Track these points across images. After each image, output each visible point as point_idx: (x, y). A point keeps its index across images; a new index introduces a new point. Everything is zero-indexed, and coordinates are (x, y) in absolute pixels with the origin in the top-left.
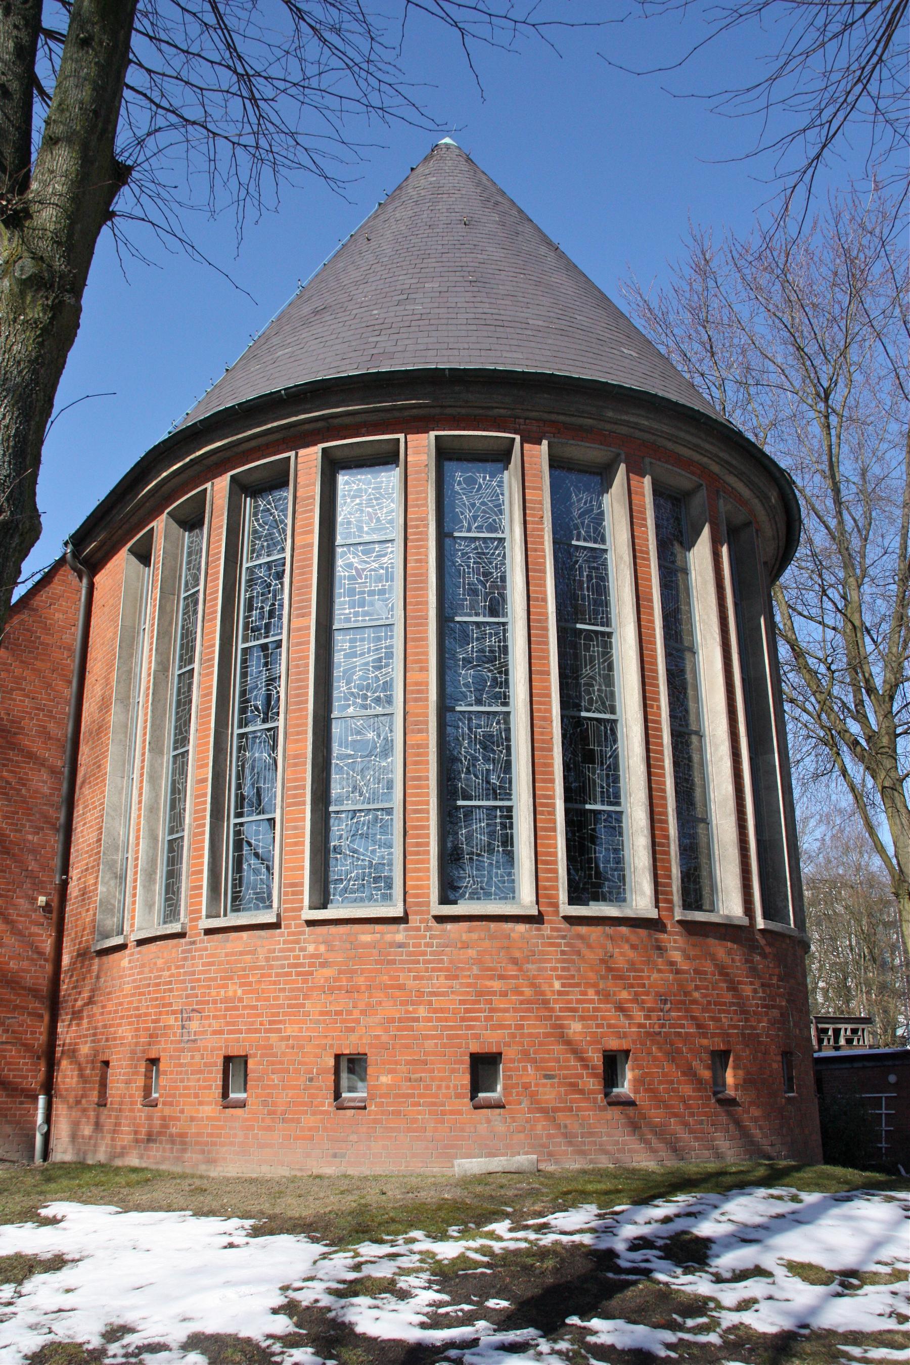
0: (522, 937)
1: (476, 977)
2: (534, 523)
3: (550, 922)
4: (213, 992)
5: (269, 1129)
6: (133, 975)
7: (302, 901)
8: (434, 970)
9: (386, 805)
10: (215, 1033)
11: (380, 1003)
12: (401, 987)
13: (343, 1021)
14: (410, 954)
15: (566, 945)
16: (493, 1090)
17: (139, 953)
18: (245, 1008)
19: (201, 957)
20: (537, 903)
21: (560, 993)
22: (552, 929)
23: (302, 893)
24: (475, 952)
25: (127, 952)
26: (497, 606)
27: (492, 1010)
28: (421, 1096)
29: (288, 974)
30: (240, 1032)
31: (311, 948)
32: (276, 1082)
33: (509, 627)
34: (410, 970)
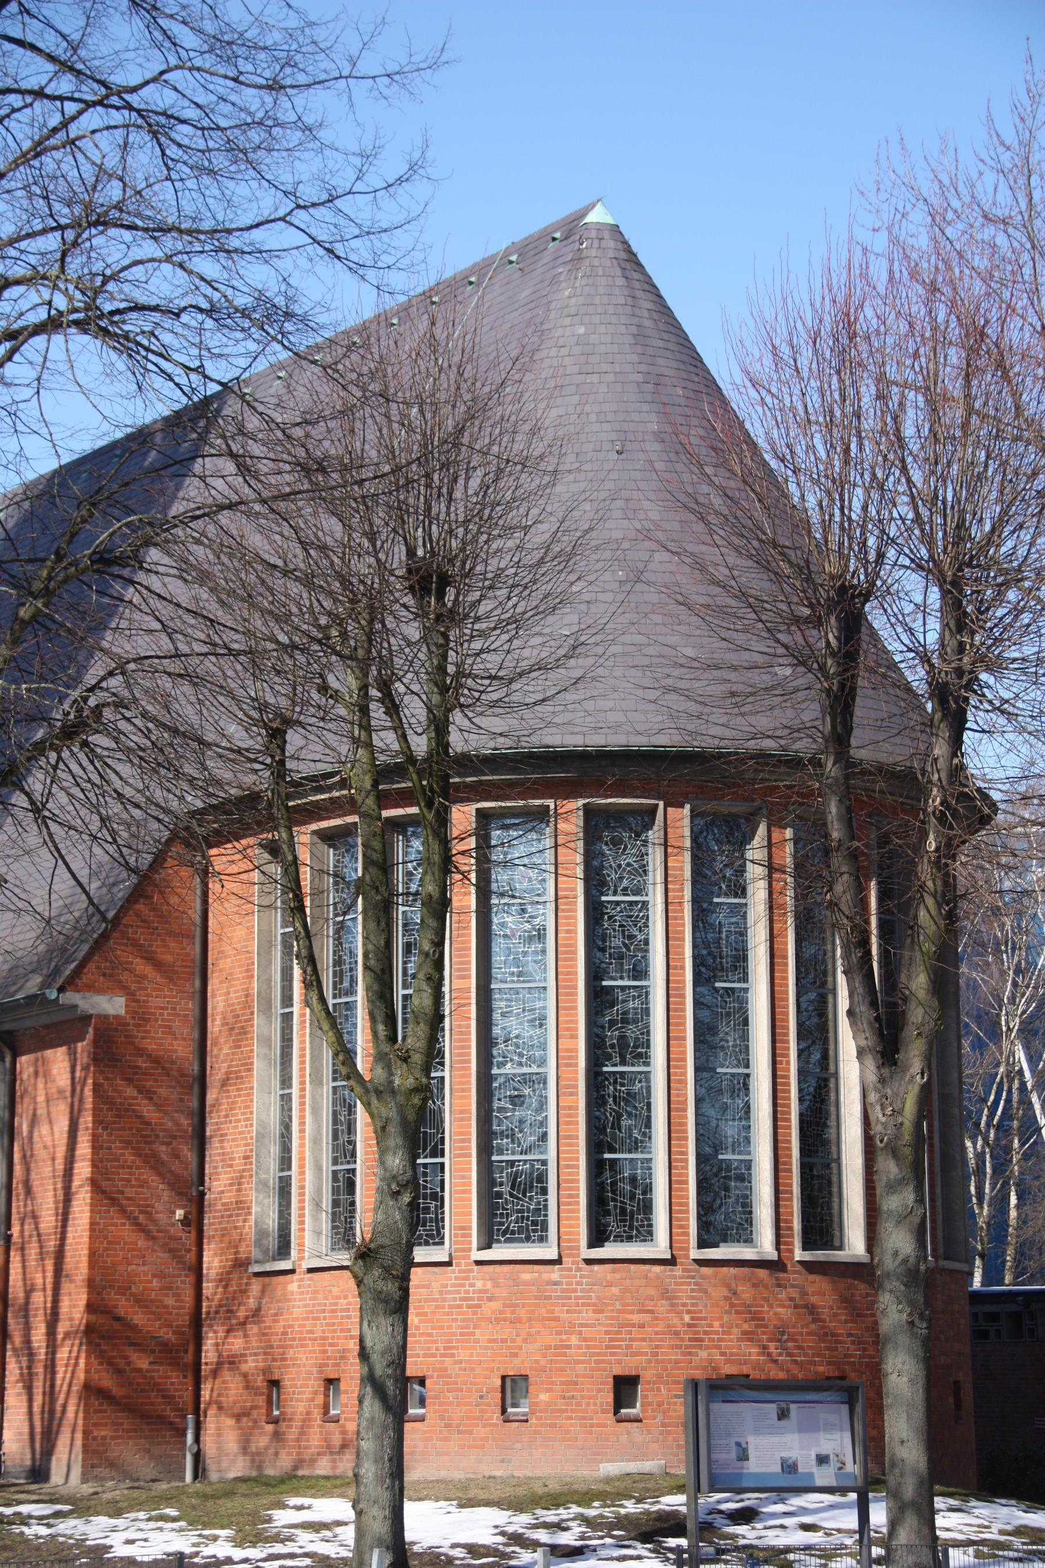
0: (658, 1277)
1: (619, 1311)
2: (674, 890)
3: (682, 1264)
5: (446, 1439)
6: (305, 1299)
7: (470, 1243)
8: (583, 1305)
9: (542, 1157)
12: (556, 1319)
13: (508, 1348)
14: (563, 1291)
15: (695, 1284)
16: (634, 1407)
17: (311, 1279)
18: (421, 1335)
20: (671, 1247)
21: (689, 1325)
23: (470, 1235)
25: (295, 1277)
26: (640, 972)
27: (631, 1340)
28: (572, 1411)
29: (460, 1306)
31: (479, 1284)
33: (651, 990)
34: (563, 1305)
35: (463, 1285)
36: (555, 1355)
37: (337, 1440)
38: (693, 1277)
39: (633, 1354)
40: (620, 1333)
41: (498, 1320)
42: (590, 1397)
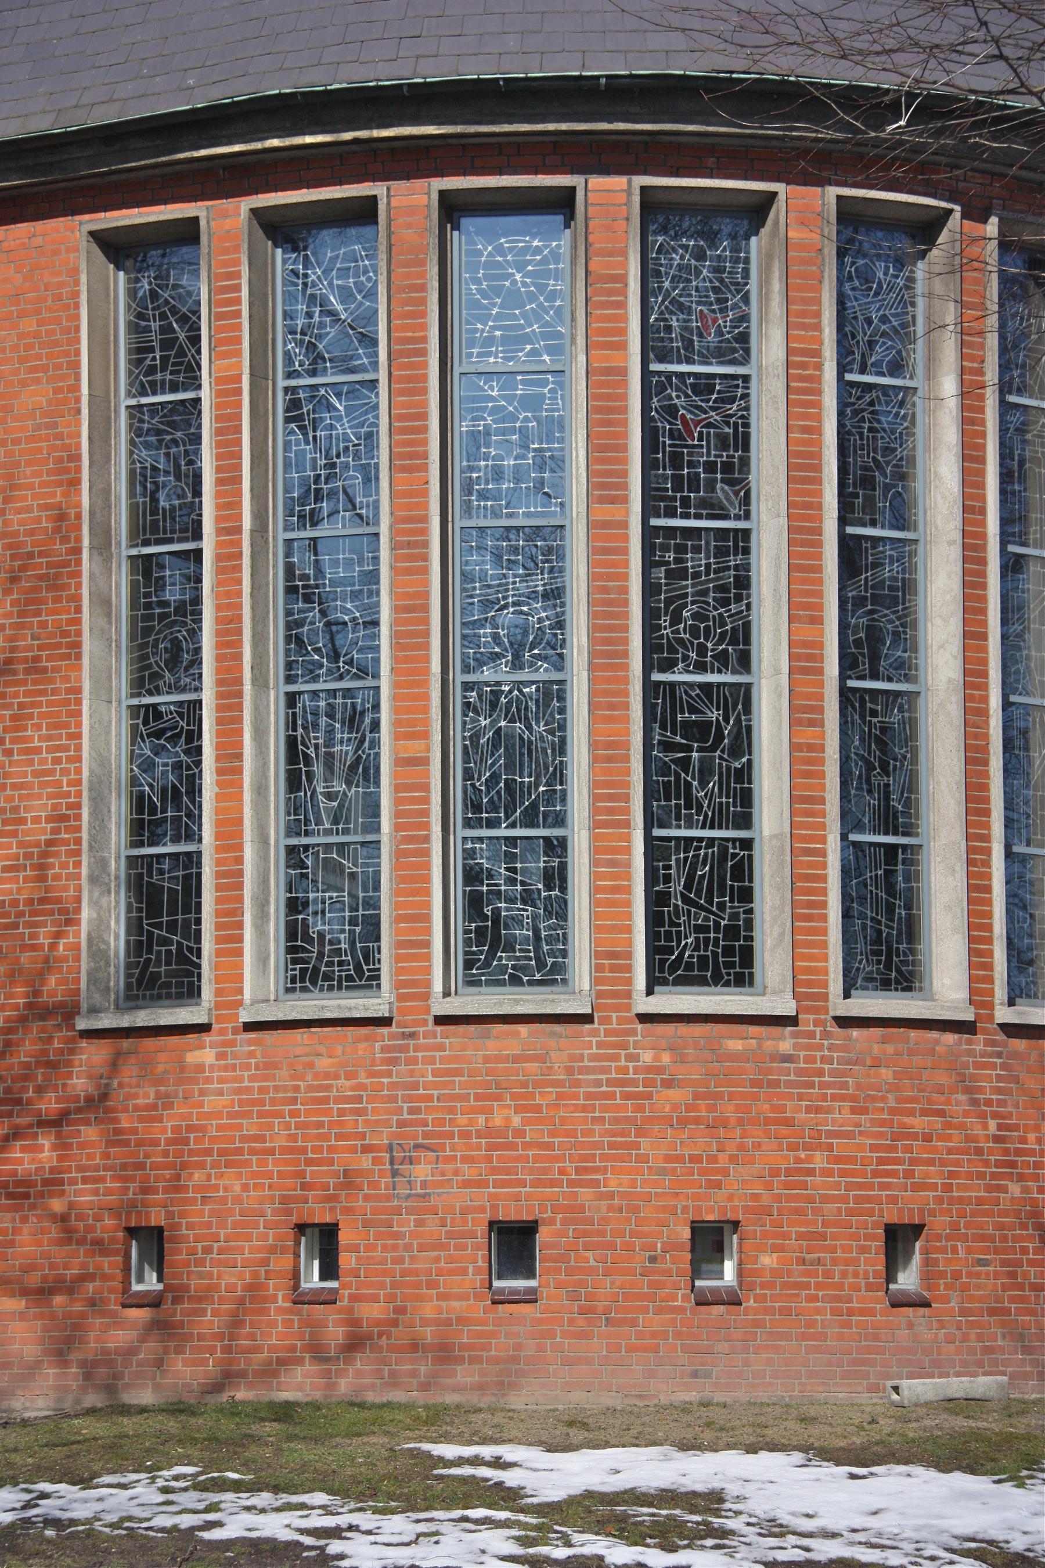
1: (892, 1111)
4: (462, 1119)
8: (834, 1097)
10: (467, 1184)
11: (758, 1146)
12: (789, 1122)
14: (800, 1072)
17: (250, 1043)
18: (527, 1146)
19: (432, 1061)
21: (997, 1139)
22: (987, 1042)
24: (890, 1073)
25: (207, 1038)
27: (913, 1162)
28: (819, 1286)
29: (612, 1096)
30: (522, 1183)
31: (647, 1057)
32: (592, 1262)
35: (616, 1058)
36: (788, 1186)
37: (335, 1333)
38: (999, 1055)
39: (916, 1188)
40: (893, 1149)
41: (683, 1122)
42: (848, 1262)
